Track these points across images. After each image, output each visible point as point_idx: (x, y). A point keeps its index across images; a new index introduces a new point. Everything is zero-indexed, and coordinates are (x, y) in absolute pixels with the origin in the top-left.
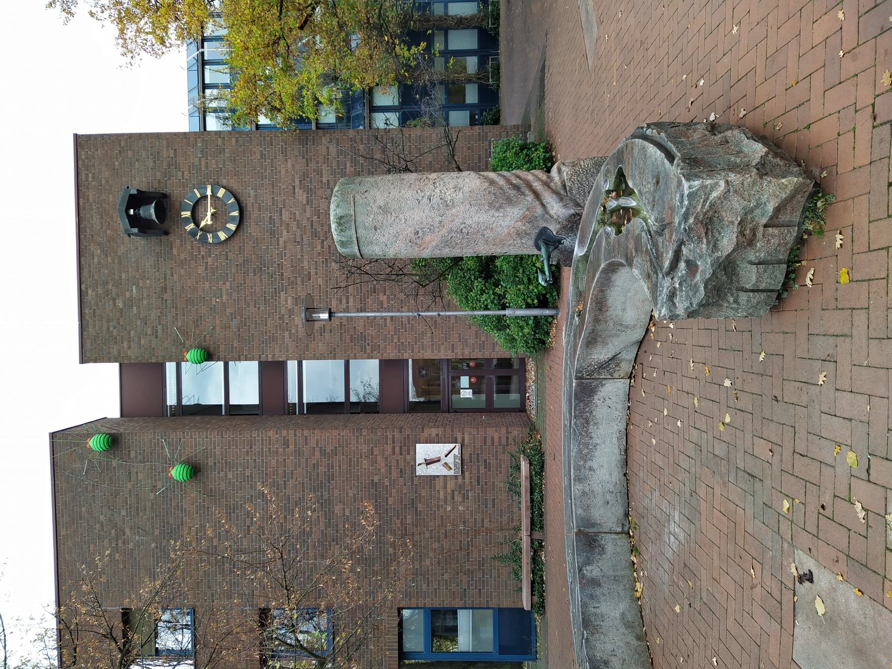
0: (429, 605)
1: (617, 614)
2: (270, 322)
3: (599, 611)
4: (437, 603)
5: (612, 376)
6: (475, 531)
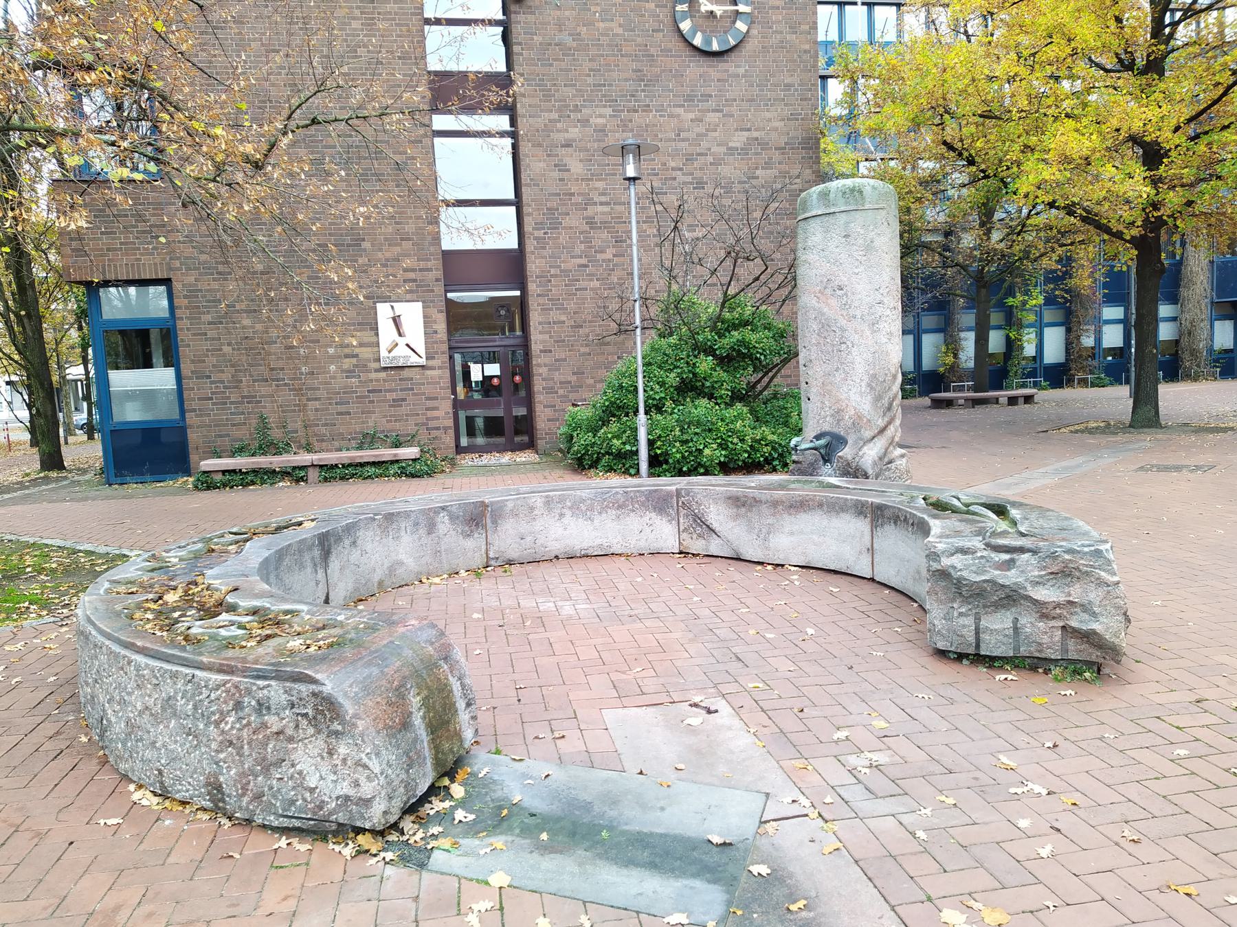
0: (179, 324)
1: (402, 557)
2: (570, 92)
3: (403, 533)
4: (184, 335)
5: (683, 531)
6: (301, 389)
